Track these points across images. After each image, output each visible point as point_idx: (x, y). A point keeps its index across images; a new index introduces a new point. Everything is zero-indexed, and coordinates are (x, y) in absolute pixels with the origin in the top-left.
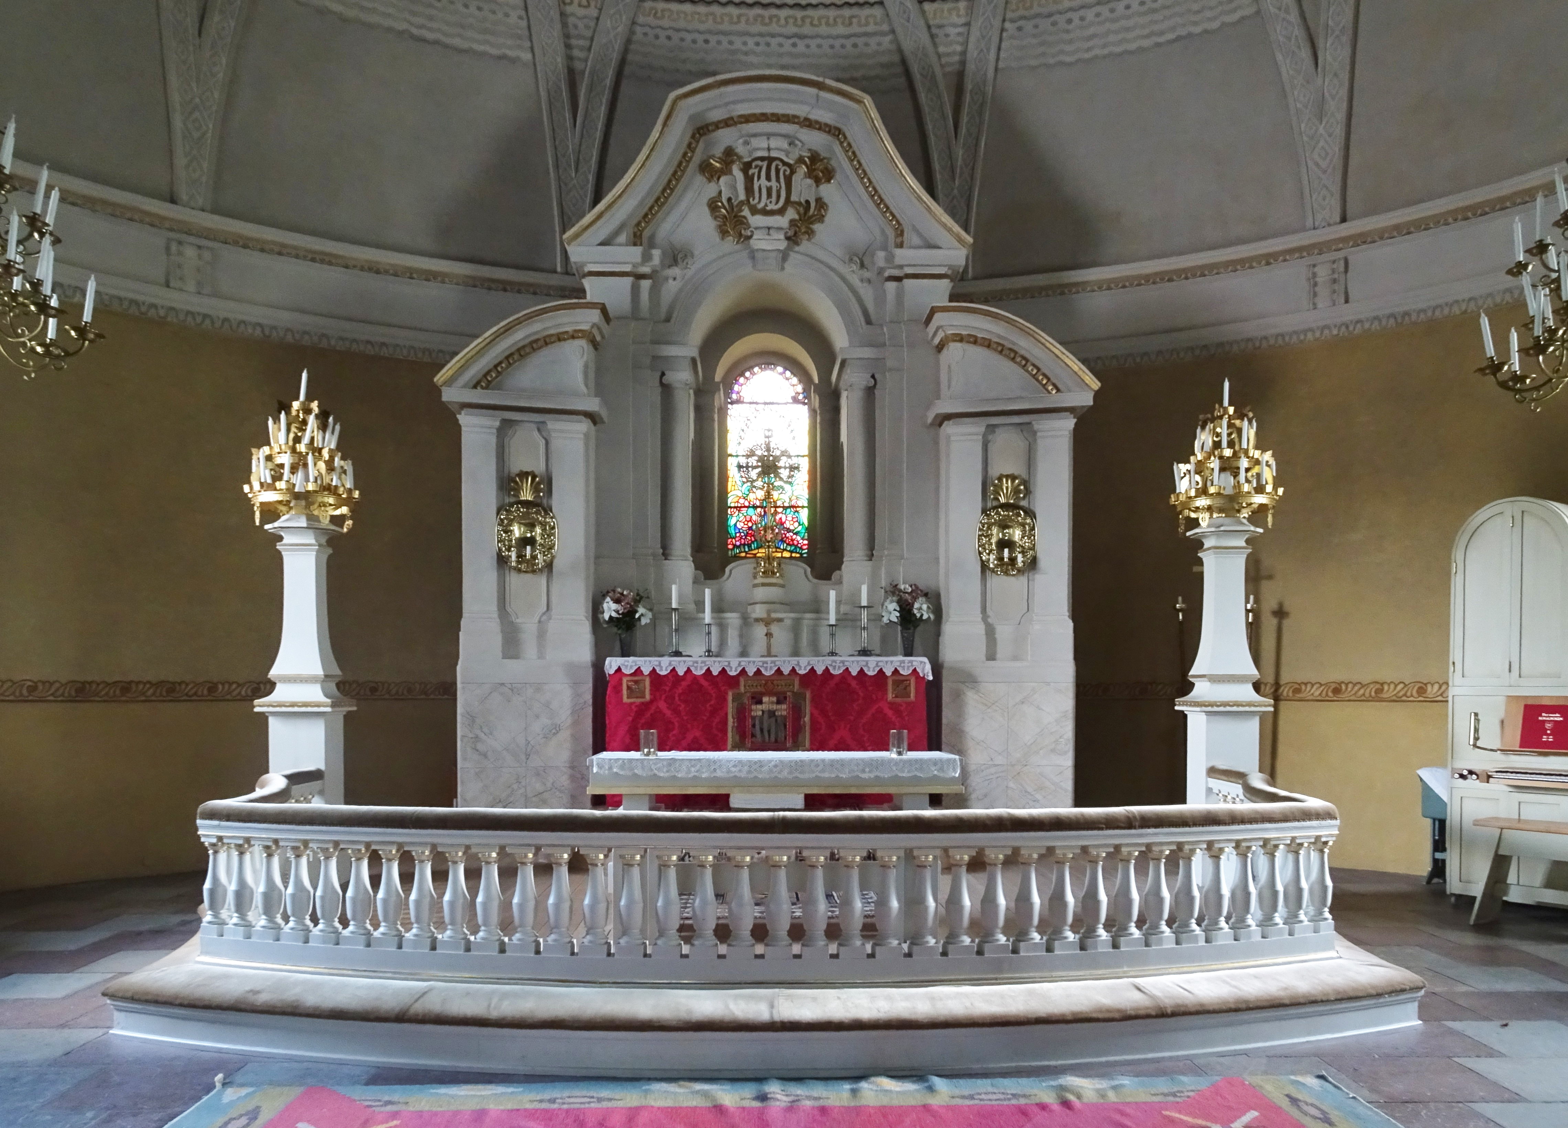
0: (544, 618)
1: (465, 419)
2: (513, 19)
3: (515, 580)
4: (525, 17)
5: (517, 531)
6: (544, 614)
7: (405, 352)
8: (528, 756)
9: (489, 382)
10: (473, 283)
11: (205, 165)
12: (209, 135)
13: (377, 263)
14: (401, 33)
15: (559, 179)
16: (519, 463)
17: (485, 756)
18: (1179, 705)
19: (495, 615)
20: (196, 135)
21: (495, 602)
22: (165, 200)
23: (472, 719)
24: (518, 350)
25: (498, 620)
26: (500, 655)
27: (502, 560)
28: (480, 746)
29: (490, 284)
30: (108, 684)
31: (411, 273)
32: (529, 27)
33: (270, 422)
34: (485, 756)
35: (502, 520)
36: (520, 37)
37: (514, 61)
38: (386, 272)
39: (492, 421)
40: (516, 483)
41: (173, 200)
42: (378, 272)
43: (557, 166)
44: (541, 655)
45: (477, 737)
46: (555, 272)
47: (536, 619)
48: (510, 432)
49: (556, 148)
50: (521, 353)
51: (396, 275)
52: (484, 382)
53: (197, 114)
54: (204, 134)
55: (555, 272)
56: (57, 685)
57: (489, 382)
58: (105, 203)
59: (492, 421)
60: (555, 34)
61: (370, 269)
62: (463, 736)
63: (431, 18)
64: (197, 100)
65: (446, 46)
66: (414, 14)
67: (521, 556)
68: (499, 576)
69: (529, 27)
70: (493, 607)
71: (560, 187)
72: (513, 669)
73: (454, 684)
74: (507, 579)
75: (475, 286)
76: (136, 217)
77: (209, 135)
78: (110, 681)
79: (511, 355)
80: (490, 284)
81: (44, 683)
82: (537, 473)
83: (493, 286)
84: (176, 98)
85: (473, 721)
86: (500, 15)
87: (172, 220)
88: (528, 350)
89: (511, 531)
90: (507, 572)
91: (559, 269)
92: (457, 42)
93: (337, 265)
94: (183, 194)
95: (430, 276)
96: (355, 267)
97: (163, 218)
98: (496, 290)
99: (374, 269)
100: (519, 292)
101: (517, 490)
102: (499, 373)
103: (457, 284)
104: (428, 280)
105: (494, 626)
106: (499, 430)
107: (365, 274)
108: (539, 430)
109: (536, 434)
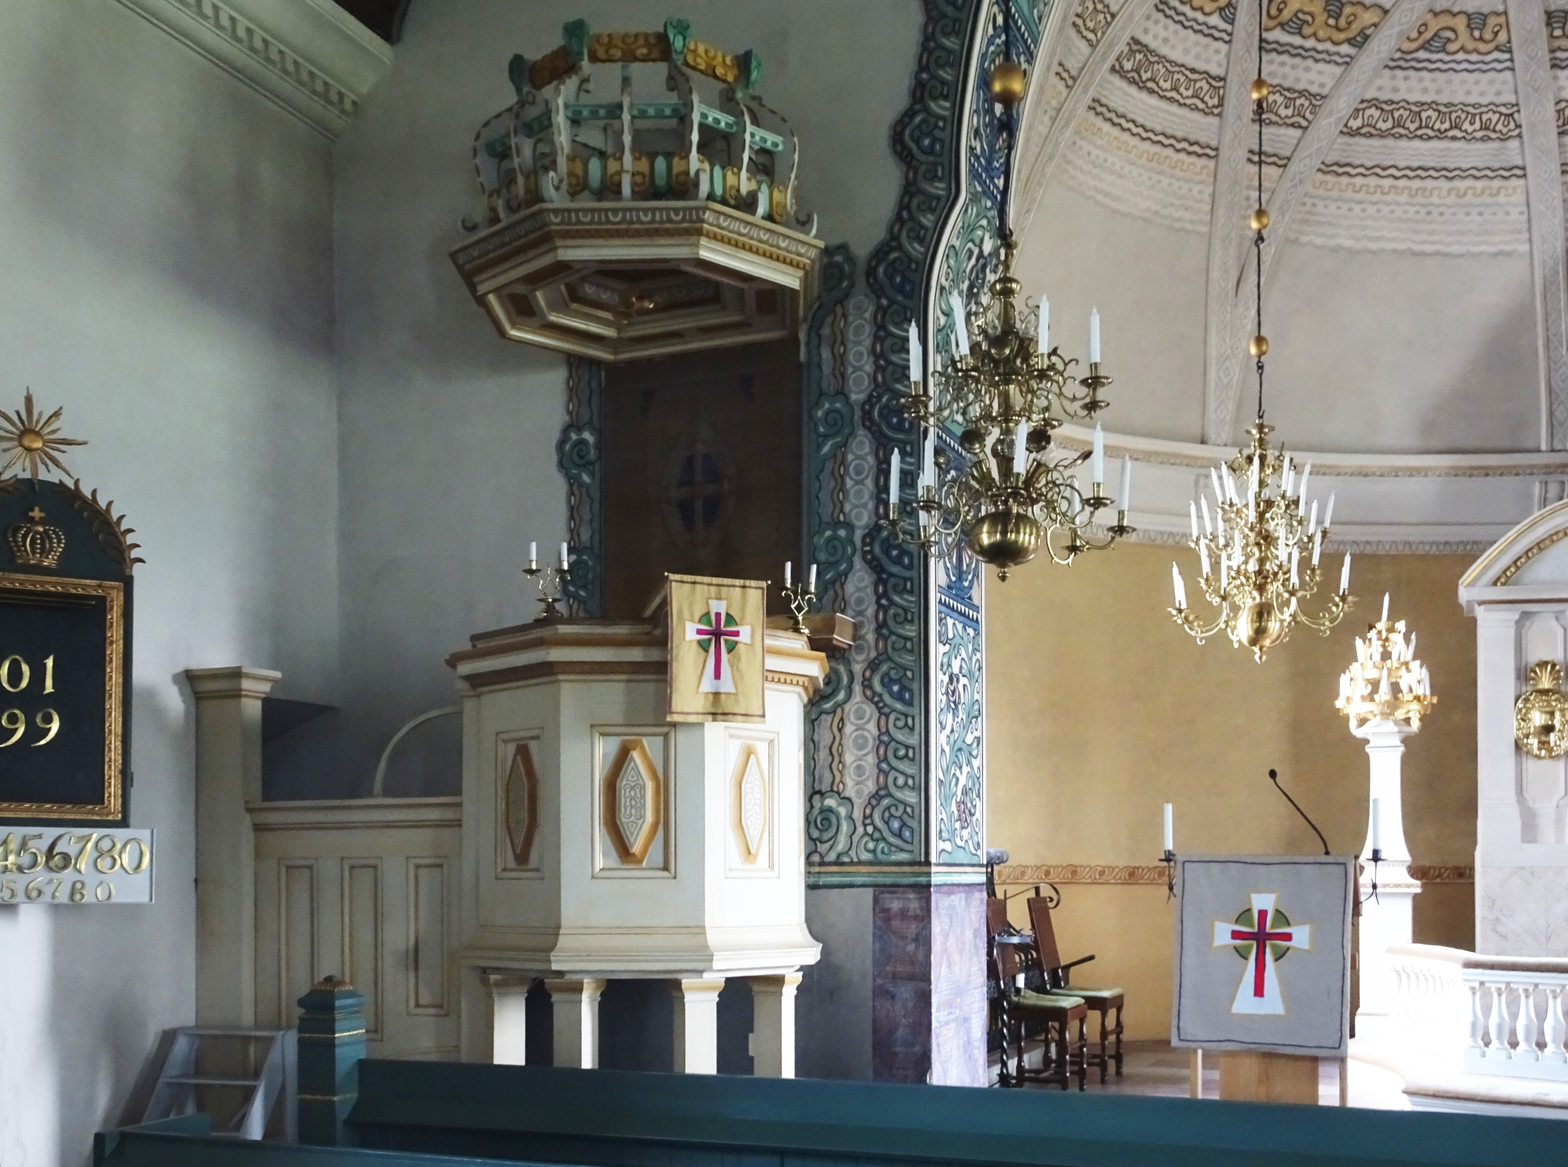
0: (1562, 802)
1: (1480, 613)
2: (1514, 215)
3: (1530, 765)
4: (1526, 211)
5: (1538, 719)
6: (1562, 798)
7: (1387, 547)
8: (1548, 939)
9: (1508, 578)
10: (1456, 472)
11: (1230, 407)
12: (1236, 378)
13: (1361, 467)
14: (1402, 252)
15: (1549, 358)
16: (1534, 656)
17: (1505, 937)
18: (556, 961)
19: (1514, 801)
20: (1225, 381)
21: (1513, 788)
22: (1196, 442)
23: (1492, 903)
24: (1538, 544)
25: (1517, 806)
26: (1519, 839)
27: (1519, 747)
28: (1499, 928)
29: (1471, 472)
30: (1149, 869)
31: (1396, 472)
32: (1529, 221)
33: (1359, 642)
34: (1505, 937)
35: (1520, 710)
36: (1519, 232)
37: (1509, 254)
38: (1374, 474)
39: (1512, 615)
40: (1535, 672)
41: (1203, 442)
42: (1366, 475)
43: (1547, 347)
44: (1560, 839)
45: (1497, 919)
46: (1539, 451)
47: (1555, 805)
48: (1528, 624)
49: (1547, 330)
50: (1540, 546)
51: (1382, 476)
52: (1503, 579)
53: (1228, 363)
54: (1232, 379)
55: (1539, 451)
56: (1117, 870)
57: (1508, 578)
58: (1157, 454)
59: (1512, 615)
60: (1557, 221)
61: (1360, 474)
62: (1483, 918)
63: (1432, 233)
64: (1229, 351)
65: (1445, 255)
66: (1418, 232)
67: (1543, 744)
68: (1516, 763)
69: (1529, 221)
70: (1511, 794)
71: (1549, 365)
72: (1532, 854)
73: (1472, 869)
74: (1524, 766)
75: (1456, 475)
76: (1178, 461)
77: (1236, 378)
78: (1151, 866)
79: (1530, 549)
80: (1471, 472)
81: (1109, 868)
82: (1556, 661)
83: (1475, 472)
84: (1213, 353)
85: (1494, 904)
86: (1500, 216)
87: (1203, 458)
88: (1547, 542)
89: (1530, 720)
90: (1524, 759)
91: (1544, 447)
92: (1456, 249)
93: (1331, 474)
94: (1212, 436)
95: (1412, 472)
96: (1346, 474)
97: (1196, 458)
98: (1478, 476)
99: (1364, 473)
100: (1501, 475)
101: (1536, 679)
102: (1518, 568)
103: (1439, 476)
104: (1411, 476)
105: (1513, 811)
106: (1517, 622)
107: (1354, 478)
108: (1557, 618)
109: (1554, 623)
